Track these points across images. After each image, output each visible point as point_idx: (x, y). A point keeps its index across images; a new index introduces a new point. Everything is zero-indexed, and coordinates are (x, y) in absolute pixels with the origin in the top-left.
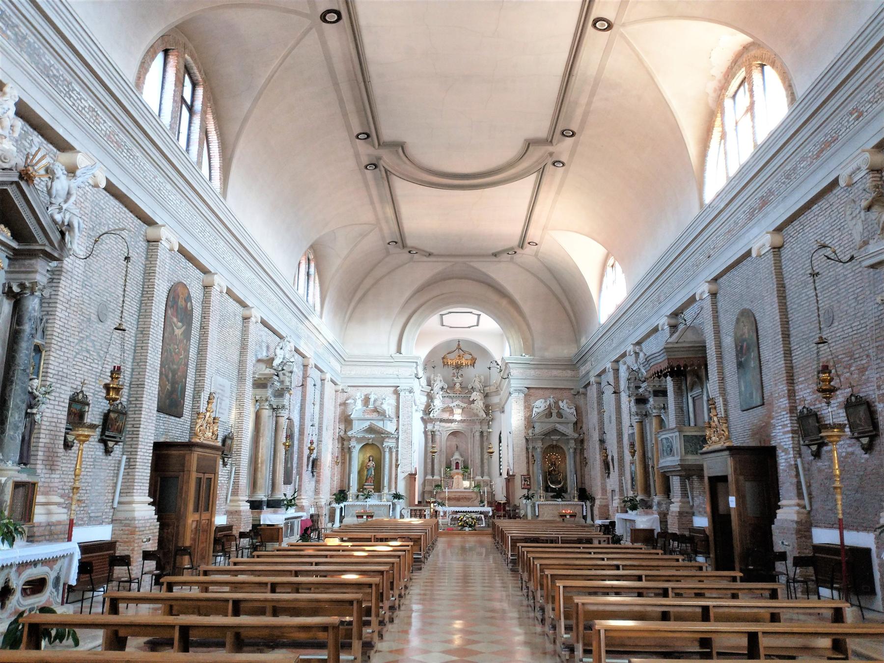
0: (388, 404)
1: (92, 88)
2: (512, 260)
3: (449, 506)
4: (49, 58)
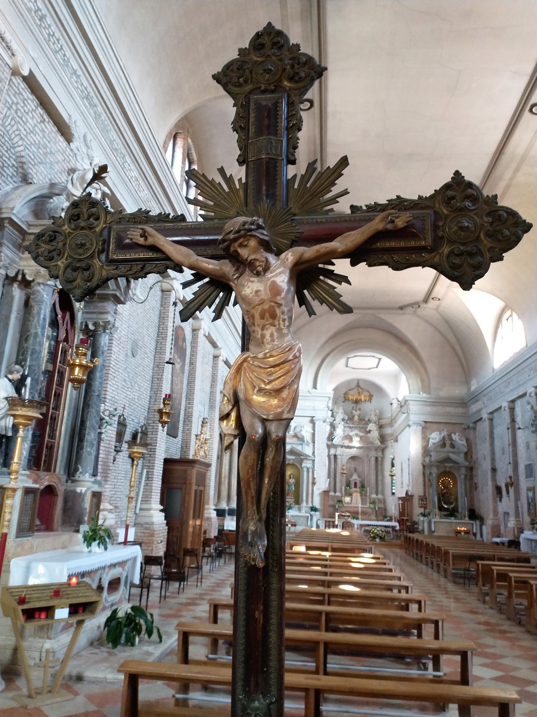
0: (306, 431)
1: (139, 161)
2: (415, 313)
3: (362, 520)
4: (113, 135)
